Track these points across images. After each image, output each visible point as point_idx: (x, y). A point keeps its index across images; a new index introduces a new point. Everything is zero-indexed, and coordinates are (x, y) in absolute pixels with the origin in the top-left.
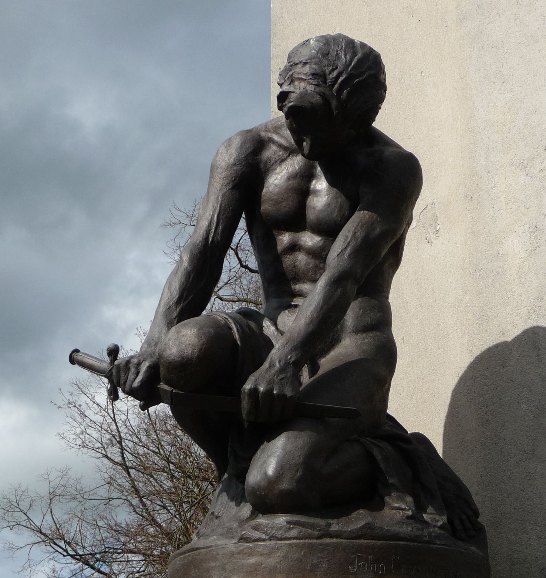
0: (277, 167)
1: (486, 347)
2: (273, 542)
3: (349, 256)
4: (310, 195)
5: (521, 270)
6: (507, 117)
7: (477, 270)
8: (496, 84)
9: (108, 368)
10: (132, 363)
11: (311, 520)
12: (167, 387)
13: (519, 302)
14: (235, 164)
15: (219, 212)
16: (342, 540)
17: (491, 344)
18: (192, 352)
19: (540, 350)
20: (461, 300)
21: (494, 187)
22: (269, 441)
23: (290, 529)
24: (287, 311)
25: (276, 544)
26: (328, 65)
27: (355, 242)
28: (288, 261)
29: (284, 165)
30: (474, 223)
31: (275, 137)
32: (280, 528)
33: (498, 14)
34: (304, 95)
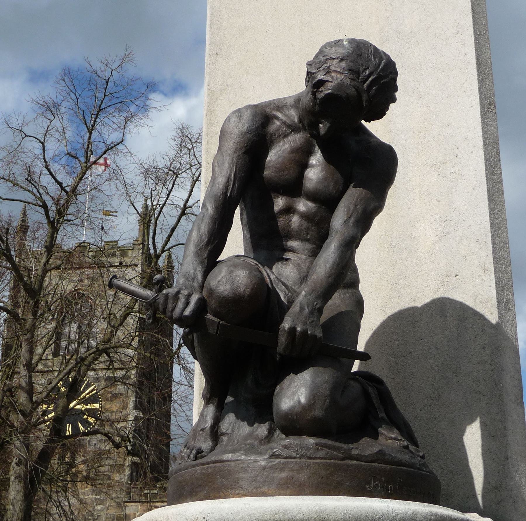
0: (281, 141)
1: (398, 309)
2: (303, 460)
3: (353, 224)
4: (308, 168)
5: (431, 251)
6: (423, 126)
7: (392, 246)
8: (414, 98)
9: (152, 296)
10: (181, 294)
11: (337, 444)
12: (214, 318)
13: (429, 276)
14: (246, 133)
15: (236, 171)
16: (361, 463)
17: (403, 308)
18: (244, 291)
19: (447, 317)
20: (376, 269)
21: (409, 180)
22: (296, 373)
23: (318, 450)
24: (280, 263)
25: (306, 462)
26: (362, 65)
27: (356, 213)
28: (281, 221)
29: (286, 140)
30: (391, 208)
31: (279, 115)
32: (309, 449)
33: (417, 42)
34: (340, 86)
